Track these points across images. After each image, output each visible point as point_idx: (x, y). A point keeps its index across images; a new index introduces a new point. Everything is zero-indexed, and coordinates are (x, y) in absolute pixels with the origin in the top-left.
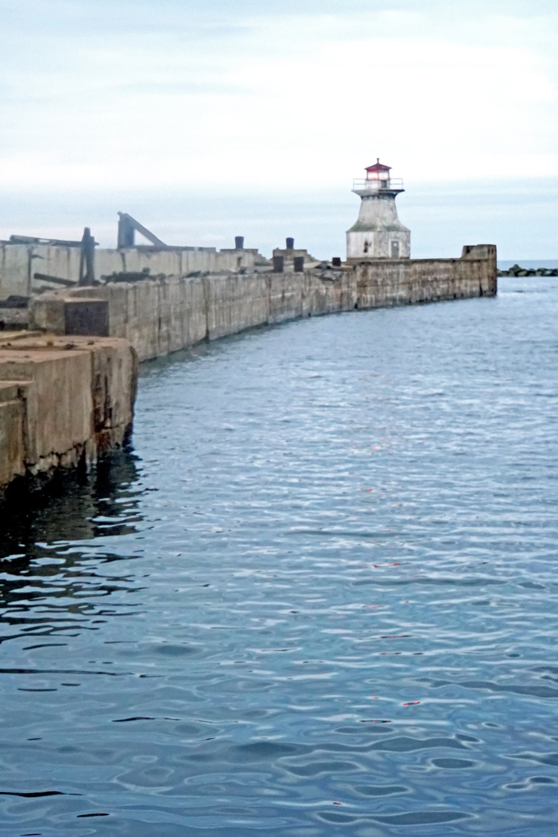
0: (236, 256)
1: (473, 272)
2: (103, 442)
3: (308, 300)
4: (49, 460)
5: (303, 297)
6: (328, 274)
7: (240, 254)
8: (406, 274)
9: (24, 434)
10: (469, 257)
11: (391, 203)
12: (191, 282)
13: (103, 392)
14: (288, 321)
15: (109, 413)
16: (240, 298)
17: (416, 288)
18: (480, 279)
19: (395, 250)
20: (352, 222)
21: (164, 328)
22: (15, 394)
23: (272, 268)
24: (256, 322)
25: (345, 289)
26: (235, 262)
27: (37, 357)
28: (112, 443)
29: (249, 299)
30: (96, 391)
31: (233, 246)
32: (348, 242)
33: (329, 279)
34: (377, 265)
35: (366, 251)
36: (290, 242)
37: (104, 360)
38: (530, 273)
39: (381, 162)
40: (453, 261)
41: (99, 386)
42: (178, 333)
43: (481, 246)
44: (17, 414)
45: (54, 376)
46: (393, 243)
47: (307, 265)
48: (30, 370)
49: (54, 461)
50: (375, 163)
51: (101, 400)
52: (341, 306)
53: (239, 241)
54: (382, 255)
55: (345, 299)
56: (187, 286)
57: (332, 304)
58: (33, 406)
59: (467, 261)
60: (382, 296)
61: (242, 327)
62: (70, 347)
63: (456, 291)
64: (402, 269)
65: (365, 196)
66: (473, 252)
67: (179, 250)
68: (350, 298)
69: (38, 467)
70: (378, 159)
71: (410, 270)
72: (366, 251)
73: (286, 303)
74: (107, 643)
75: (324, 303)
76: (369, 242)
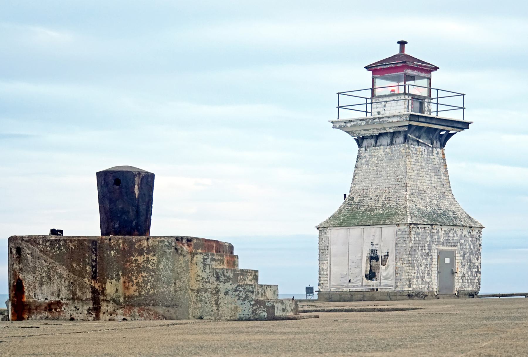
11: (436, 159)
19: (448, 273)
31: (84, 221)
35: (371, 275)
46: (441, 255)
50: (396, 50)
53: (125, 197)
65: (367, 137)
70: (402, 44)
74: (38, 327)
76: (381, 254)
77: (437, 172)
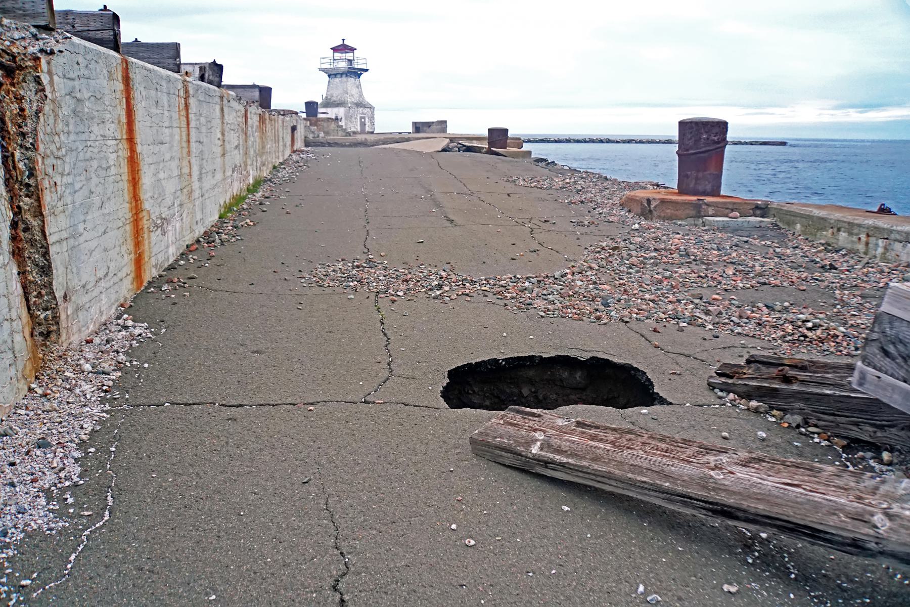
19: (363, 125)
31: (666, 169)
39: (346, 43)
46: (361, 118)
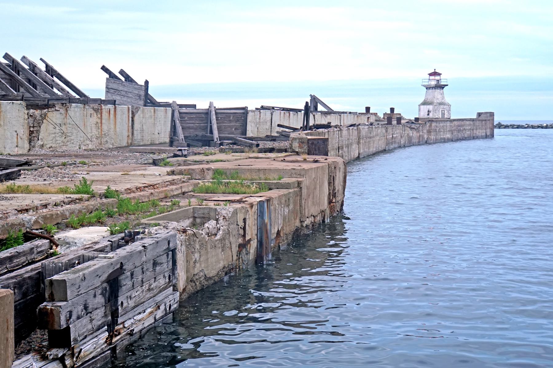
0: (367, 116)
1: (482, 126)
2: (332, 209)
3: (403, 138)
4: (310, 219)
5: (401, 137)
6: (413, 126)
7: (369, 116)
8: (451, 126)
9: (301, 206)
10: (480, 118)
12: (353, 129)
13: (332, 184)
14: (395, 148)
15: (334, 195)
16: (373, 137)
17: (455, 133)
18: (486, 129)
19: (443, 114)
20: (422, 100)
21: (341, 152)
22: (296, 185)
23: (386, 122)
24: (380, 149)
25: (421, 133)
26: (366, 119)
27: (306, 166)
28: (336, 210)
29: (378, 138)
30: (329, 183)
31: (364, 111)
32: (419, 110)
33: (413, 128)
34: (436, 122)
35: (428, 115)
36: (392, 110)
37: (333, 168)
38: (506, 127)
40: (473, 120)
41: (331, 181)
42: (347, 154)
43: (486, 113)
44: (298, 195)
45: (313, 176)
46: (442, 111)
47: (402, 121)
48: (302, 173)
49: (312, 219)
51: (332, 188)
52: (419, 142)
53: (368, 109)
54: (437, 117)
55: (421, 139)
56: (351, 131)
57: (415, 140)
58: (304, 191)
59: (479, 120)
60: (439, 137)
61: (374, 152)
62: (316, 161)
63: (474, 135)
64: (448, 124)
66: (482, 116)
67: (340, 113)
68: (423, 138)
69: (306, 223)
71: (453, 124)
72: (428, 115)
73: (394, 140)
75: (411, 140)
77: (441, 94)
